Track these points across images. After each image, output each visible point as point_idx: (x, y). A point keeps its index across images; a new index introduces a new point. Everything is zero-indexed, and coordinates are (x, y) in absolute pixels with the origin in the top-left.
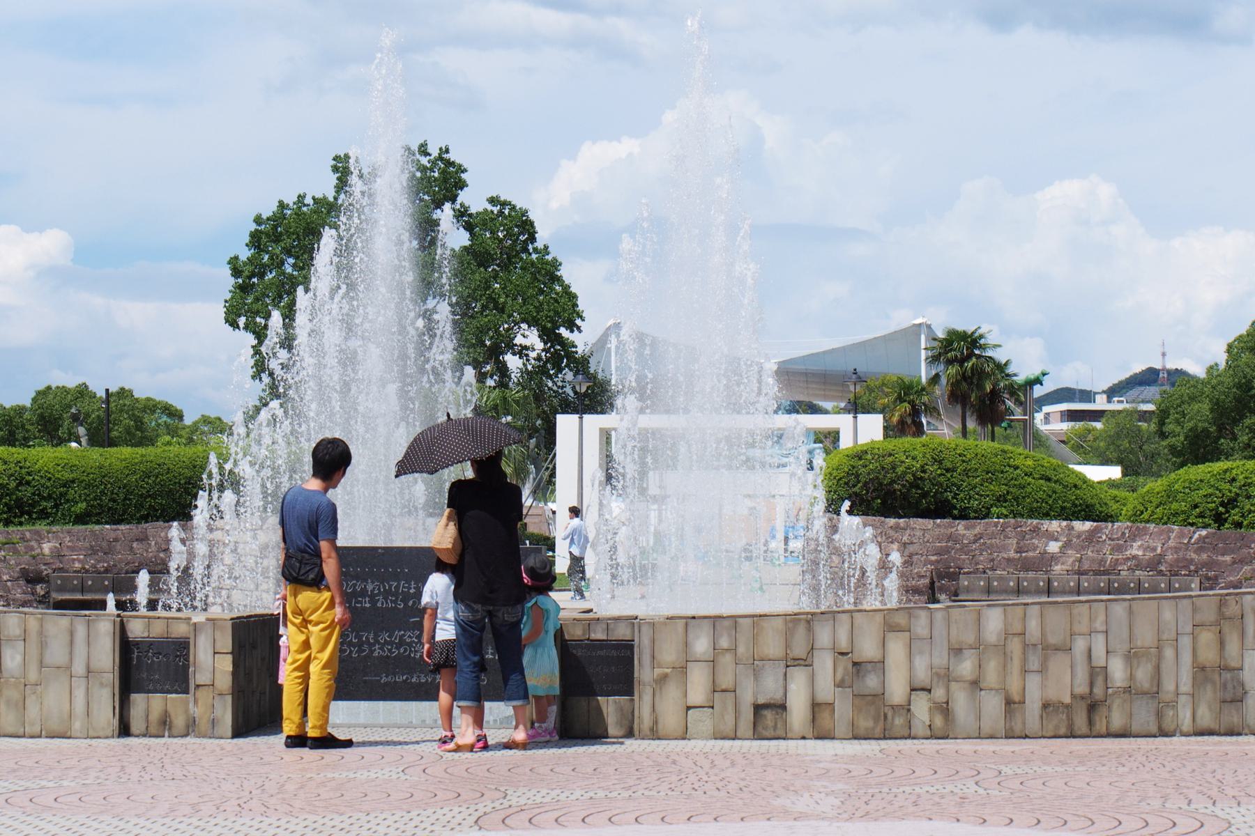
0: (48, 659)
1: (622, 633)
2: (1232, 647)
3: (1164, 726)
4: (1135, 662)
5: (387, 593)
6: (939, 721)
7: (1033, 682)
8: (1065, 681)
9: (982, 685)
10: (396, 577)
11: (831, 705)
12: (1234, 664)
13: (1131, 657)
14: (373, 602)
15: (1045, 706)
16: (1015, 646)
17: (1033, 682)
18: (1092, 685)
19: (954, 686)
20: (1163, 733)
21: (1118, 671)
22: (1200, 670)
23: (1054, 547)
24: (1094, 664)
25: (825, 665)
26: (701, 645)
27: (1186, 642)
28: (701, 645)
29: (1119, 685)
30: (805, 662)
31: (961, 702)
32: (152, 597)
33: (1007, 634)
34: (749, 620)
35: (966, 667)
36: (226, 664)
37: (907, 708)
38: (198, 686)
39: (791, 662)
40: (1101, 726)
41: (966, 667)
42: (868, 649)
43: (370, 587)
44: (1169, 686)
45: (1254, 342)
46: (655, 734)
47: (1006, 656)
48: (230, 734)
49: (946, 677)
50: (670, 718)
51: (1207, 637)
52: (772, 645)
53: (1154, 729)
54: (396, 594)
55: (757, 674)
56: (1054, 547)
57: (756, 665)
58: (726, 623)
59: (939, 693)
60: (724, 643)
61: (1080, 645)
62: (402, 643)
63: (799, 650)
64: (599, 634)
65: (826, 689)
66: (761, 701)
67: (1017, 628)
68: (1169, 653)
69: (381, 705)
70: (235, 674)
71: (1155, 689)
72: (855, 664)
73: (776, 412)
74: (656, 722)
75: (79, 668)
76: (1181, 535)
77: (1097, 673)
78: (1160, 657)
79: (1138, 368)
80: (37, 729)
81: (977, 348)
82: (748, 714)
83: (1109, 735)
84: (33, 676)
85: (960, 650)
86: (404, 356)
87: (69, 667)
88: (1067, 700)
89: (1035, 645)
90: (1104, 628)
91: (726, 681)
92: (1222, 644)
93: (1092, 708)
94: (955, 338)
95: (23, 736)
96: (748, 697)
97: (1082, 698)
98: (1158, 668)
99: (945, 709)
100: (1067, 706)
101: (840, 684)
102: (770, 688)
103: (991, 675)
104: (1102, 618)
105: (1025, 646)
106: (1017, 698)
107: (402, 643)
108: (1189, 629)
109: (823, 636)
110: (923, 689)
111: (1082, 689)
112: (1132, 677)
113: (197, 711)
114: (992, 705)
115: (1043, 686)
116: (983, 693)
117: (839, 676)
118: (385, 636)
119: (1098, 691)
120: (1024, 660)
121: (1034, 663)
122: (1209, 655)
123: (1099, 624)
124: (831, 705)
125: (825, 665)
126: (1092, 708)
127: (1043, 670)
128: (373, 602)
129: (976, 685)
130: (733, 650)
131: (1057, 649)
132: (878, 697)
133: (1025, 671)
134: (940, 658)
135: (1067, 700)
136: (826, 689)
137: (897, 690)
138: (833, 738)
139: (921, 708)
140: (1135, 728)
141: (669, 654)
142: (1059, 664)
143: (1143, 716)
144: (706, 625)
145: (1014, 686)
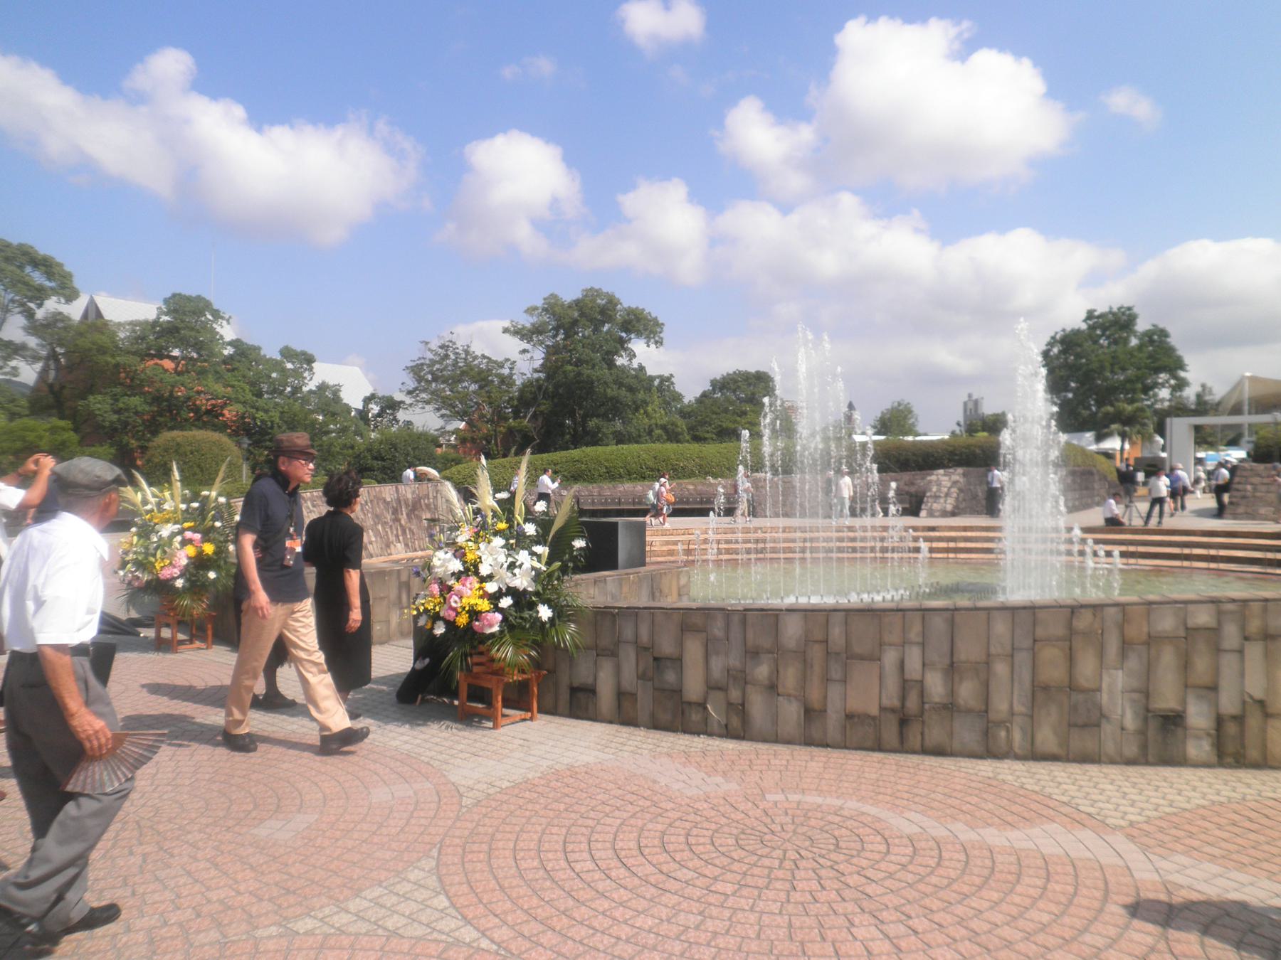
4: (957, 678)
6: (735, 722)
7: (834, 692)
9: (781, 690)
11: (633, 695)
13: (952, 670)
16: (816, 652)
18: (903, 698)
19: (749, 688)
21: (936, 686)
22: (1040, 691)
24: (907, 676)
25: (629, 658)
27: (1023, 658)
29: (937, 699)
30: (613, 654)
31: (758, 706)
32: (1199, 748)
35: (762, 671)
37: (702, 706)
40: (914, 739)
41: (762, 671)
42: (666, 646)
47: (806, 664)
49: (741, 678)
59: (735, 695)
61: (890, 657)
63: (605, 641)
66: (575, 684)
67: (818, 635)
71: (983, 708)
72: (655, 659)
81: (1148, 475)
85: (757, 653)
86: (688, 502)
88: (874, 711)
89: (838, 654)
90: (920, 640)
93: (904, 722)
97: (893, 710)
98: (986, 685)
99: (741, 709)
100: (874, 718)
101: (642, 677)
103: (790, 678)
106: (817, 706)
108: (1027, 643)
110: (720, 689)
111: (891, 699)
112: (952, 693)
114: (791, 712)
116: (781, 698)
117: (641, 669)
119: (912, 703)
124: (633, 695)
125: (629, 658)
129: (772, 688)
131: (862, 658)
132: (677, 692)
133: (826, 680)
137: (693, 686)
140: (956, 745)
145: (814, 695)
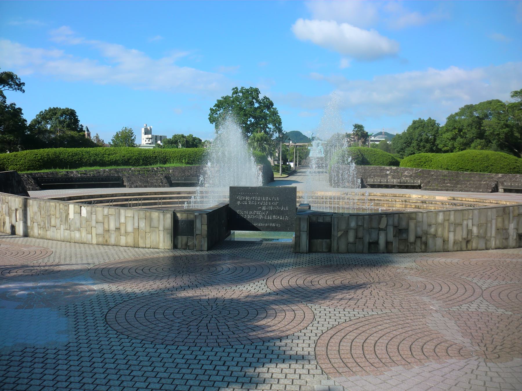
0: (152, 225)
1: (328, 219)
2: (506, 222)
3: (487, 246)
5: (252, 200)
8: (460, 234)
10: (254, 195)
11: (392, 243)
12: (507, 228)
13: (479, 226)
14: (248, 203)
15: (454, 242)
16: (446, 224)
18: (468, 235)
20: (487, 249)
21: (475, 230)
23: (388, 172)
26: (353, 224)
28: (353, 224)
30: (385, 230)
33: (444, 220)
34: (367, 216)
36: (205, 227)
38: (197, 235)
40: (469, 247)
43: (247, 199)
44: (489, 235)
46: (338, 252)
47: (444, 228)
48: (206, 249)
51: (500, 220)
53: (484, 248)
54: (254, 200)
56: (388, 172)
58: (361, 217)
62: (256, 214)
64: (321, 220)
65: (391, 237)
66: (371, 241)
67: (447, 218)
68: (489, 225)
70: (208, 231)
73: (313, 139)
74: (338, 248)
76: (416, 170)
77: (470, 232)
78: (487, 226)
79: (379, 131)
80: (149, 247)
82: (366, 245)
83: (472, 250)
88: (461, 240)
91: (360, 235)
92: (504, 221)
94: (212, 120)
95: (146, 248)
96: (367, 239)
101: (394, 236)
102: (374, 236)
104: (471, 215)
105: (449, 223)
107: (256, 214)
108: (495, 217)
111: (465, 236)
113: (196, 242)
115: (455, 236)
118: (251, 212)
120: (449, 228)
121: (452, 229)
122: (500, 225)
123: (470, 217)
124: (392, 243)
126: (468, 242)
127: (454, 231)
128: (248, 203)
130: (363, 226)
132: (406, 240)
133: (449, 231)
135: (461, 240)
136: (391, 237)
138: (392, 253)
142: (459, 229)
143: (482, 245)
144: (355, 218)
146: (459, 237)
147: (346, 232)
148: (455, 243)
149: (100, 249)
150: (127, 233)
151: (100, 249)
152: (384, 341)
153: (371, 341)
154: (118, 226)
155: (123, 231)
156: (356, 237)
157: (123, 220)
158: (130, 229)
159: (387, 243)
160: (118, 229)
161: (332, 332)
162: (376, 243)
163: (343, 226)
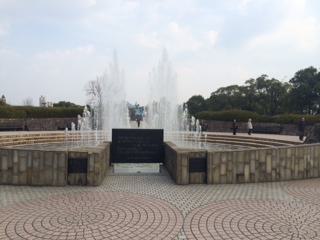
8: (302, 166)
17: (297, 167)
25: (253, 163)
26: (224, 159)
28: (224, 159)
30: (249, 163)
37: (271, 174)
39: (245, 163)
41: (283, 164)
42: (263, 159)
45: (306, 77)
49: (279, 166)
50: (216, 178)
52: (241, 159)
55: (237, 167)
57: (237, 164)
60: (230, 158)
63: (247, 160)
64: (197, 156)
69: (141, 165)
75: (55, 166)
77: (308, 164)
84: (42, 167)
87: (52, 167)
93: (307, 171)
102: (240, 170)
103: (288, 165)
109: (253, 156)
125: (253, 163)
126: (307, 171)
129: (285, 168)
130: (232, 160)
132: (265, 172)
134: (278, 161)
139: (274, 174)
141: (216, 161)
142: (301, 161)
146: (302, 169)
147: (219, 166)
148: (299, 172)
149: (283, 196)
150: (20, 172)
151: (283, 196)
152: (12, 226)
153: (220, 220)
154: (11, 165)
155: (15, 170)
156: (227, 170)
157: (16, 160)
158: (23, 168)
159: (251, 174)
160: (10, 169)
161: (191, 216)
162: (243, 175)
163: (216, 161)
